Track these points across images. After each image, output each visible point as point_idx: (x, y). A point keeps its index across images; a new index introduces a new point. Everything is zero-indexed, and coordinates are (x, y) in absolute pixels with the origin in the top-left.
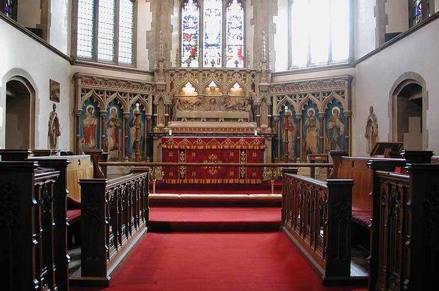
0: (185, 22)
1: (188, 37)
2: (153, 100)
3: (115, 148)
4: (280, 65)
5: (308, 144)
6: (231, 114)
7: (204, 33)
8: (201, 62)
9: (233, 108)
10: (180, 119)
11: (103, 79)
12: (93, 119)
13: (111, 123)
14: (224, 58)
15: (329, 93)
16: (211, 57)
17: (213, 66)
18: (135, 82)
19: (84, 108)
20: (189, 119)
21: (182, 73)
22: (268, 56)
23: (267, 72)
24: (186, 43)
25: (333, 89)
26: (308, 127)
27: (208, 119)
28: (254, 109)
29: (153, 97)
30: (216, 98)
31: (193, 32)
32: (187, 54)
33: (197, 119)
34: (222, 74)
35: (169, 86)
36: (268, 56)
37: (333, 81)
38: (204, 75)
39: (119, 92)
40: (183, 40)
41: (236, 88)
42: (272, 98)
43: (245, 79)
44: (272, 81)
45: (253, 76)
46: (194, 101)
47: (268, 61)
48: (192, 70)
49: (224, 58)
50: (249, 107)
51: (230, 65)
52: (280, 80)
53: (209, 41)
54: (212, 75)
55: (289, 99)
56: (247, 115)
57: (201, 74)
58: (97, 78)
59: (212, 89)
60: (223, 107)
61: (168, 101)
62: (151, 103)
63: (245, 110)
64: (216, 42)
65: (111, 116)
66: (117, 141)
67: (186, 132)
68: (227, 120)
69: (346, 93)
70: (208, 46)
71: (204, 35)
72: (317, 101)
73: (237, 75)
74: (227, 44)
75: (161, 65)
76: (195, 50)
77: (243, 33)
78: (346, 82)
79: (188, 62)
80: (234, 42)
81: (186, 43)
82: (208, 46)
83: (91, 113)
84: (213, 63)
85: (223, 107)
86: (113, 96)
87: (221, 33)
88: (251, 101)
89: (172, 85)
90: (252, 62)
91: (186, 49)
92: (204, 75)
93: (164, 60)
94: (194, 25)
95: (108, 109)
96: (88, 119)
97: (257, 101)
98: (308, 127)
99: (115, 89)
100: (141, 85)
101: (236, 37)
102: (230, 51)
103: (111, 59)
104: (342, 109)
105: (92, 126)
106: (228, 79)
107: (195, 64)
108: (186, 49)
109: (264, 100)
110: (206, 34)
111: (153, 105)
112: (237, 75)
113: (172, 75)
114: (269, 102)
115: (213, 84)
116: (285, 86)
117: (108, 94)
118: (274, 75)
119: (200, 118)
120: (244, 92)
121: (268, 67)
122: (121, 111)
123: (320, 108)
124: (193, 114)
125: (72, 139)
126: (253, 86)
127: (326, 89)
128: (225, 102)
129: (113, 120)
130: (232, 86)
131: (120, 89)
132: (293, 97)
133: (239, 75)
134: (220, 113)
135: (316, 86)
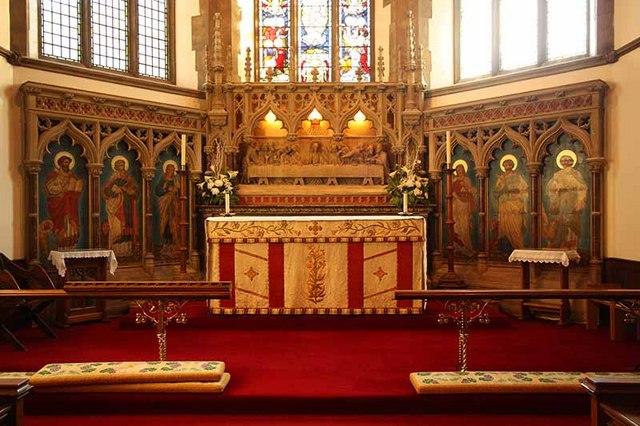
0: (264, 5)
1: (271, 33)
2: (204, 143)
3: (125, 237)
4: (438, 76)
5: (501, 226)
6: (350, 170)
7: (300, 25)
8: (293, 75)
9: (353, 159)
10: (254, 181)
11: (91, 98)
12: (72, 180)
13: (115, 188)
14: (334, 67)
15: (550, 124)
16: (312, 65)
17: (315, 79)
18: (166, 109)
19: (48, 159)
20: (272, 180)
21: (257, 93)
22: (419, 57)
23: (416, 90)
24: (268, 43)
25: (559, 113)
26: (501, 192)
27: (306, 181)
28: (391, 164)
29: (204, 140)
30: (323, 141)
31: (280, 22)
32: (271, 63)
33: (285, 180)
34: (331, 93)
35: (233, 119)
36: (418, 58)
37: (564, 96)
38: (299, 97)
39: (141, 130)
40: (261, 37)
41: (359, 121)
42: (426, 141)
43: (375, 105)
44: (426, 106)
45: (390, 98)
46: (280, 147)
47: (418, 69)
48: (276, 87)
49: (334, 67)
50: (384, 156)
51: (349, 78)
52: (438, 102)
53: (309, 40)
54: (314, 97)
55: (511, 134)
56: (379, 172)
57: (299, 95)
58: (75, 95)
59: (315, 124)
60: (333, 157)
61: (230, 146)
62: (200, 149)
63: (375, 163)
64: (321, 41)
65: (116, 175)
66: (129, 224)
67: (266, 204)
68: (341, 181)
69: (594, 122)
70: (306, 48)
71: (300, 29)
72: (471, 147)
73: (359, 97)
74: (341, 44)
75: (218, 78)
76: (284, 56)
77: (369, 24)
78: (596, 97)
79: (271, 74)
80: (354, 41)
81: (268, 43)
82: (306, 48)
83: (65, 168)
84: (315, 73)
85: (333, 157)
86: (118, 135)
87: (330, 24)
88: (387, 148)
89: (239, 117)
90: (387, 72)
91: (269, 54)
92: (299, 97)
93: (227, 66)
94: (282, 11)
95: (107, 162)
96: (59, 180)
97: (398, 144)
98: (501, 192)
99: (119, 121)
100: (177, 114)
101: (356, 32)
102: (347, 57)
103: (123, 66)
104: (471, 164)
105: (70, 195)
106: (343, 105)
107: (282, 78)
108: (269, 54)
109: (411, 142)
110: (303, 28)
111: (204, 155)
112: (359, 97)
113: (239, 98)
114: (420, 146)
115: (315, 115)
116: (453, 113)
117: (104, 129)
118: (429, 95)
119: (293, 179)
120: (374, 128)
121: (418, 80)
122: (136, 165)
123: (529, 154)
124: (279, 171)
125: (20, 222)
126: (390, 118)
127: (489, 123)
128: (341, 147)
129: (119, 182)
130: (351, 117)
131: (133, 123)
132: (469, 135)
133: (364, 97)
134: (333, 169)
135: (519, 110)
